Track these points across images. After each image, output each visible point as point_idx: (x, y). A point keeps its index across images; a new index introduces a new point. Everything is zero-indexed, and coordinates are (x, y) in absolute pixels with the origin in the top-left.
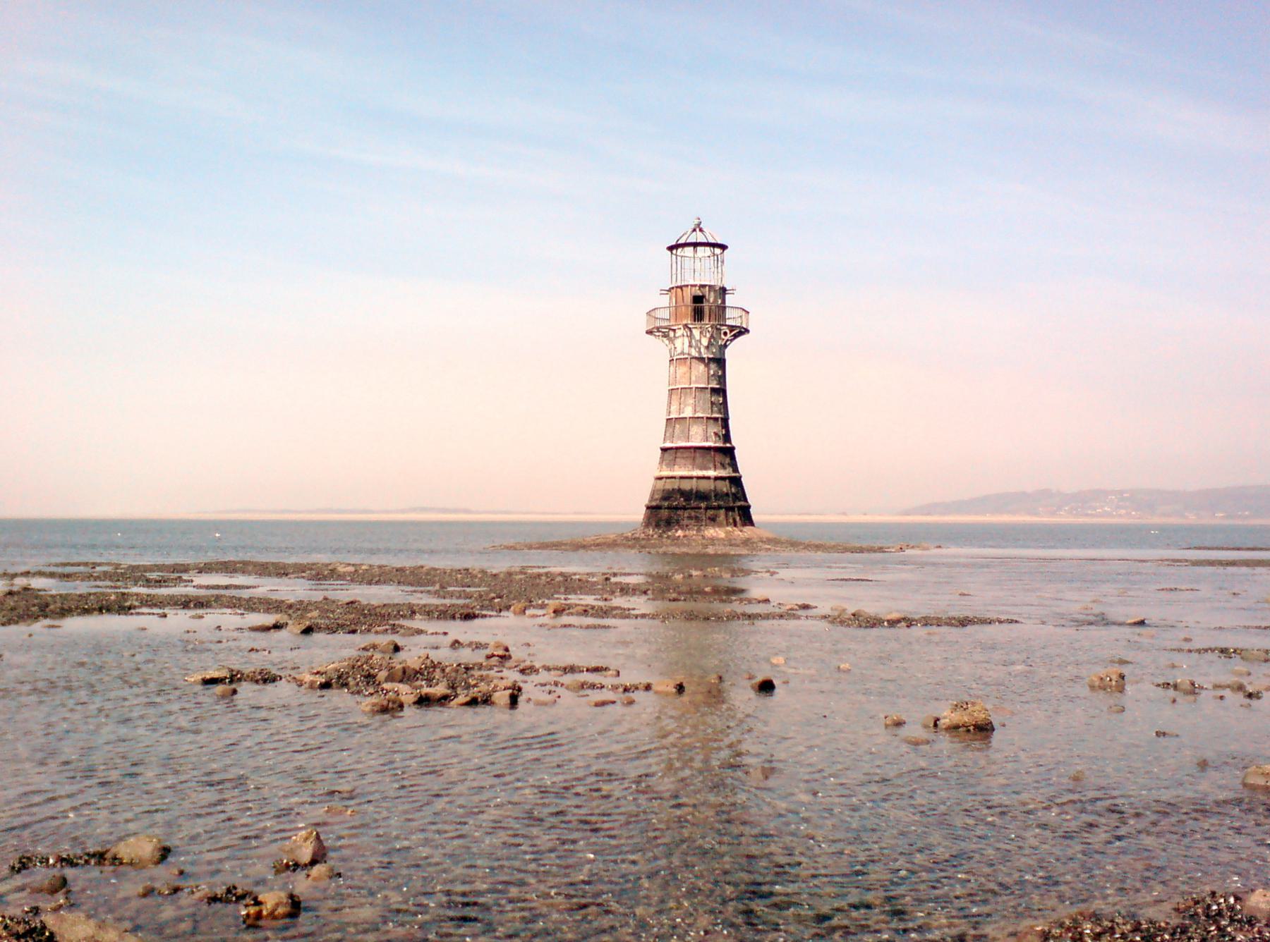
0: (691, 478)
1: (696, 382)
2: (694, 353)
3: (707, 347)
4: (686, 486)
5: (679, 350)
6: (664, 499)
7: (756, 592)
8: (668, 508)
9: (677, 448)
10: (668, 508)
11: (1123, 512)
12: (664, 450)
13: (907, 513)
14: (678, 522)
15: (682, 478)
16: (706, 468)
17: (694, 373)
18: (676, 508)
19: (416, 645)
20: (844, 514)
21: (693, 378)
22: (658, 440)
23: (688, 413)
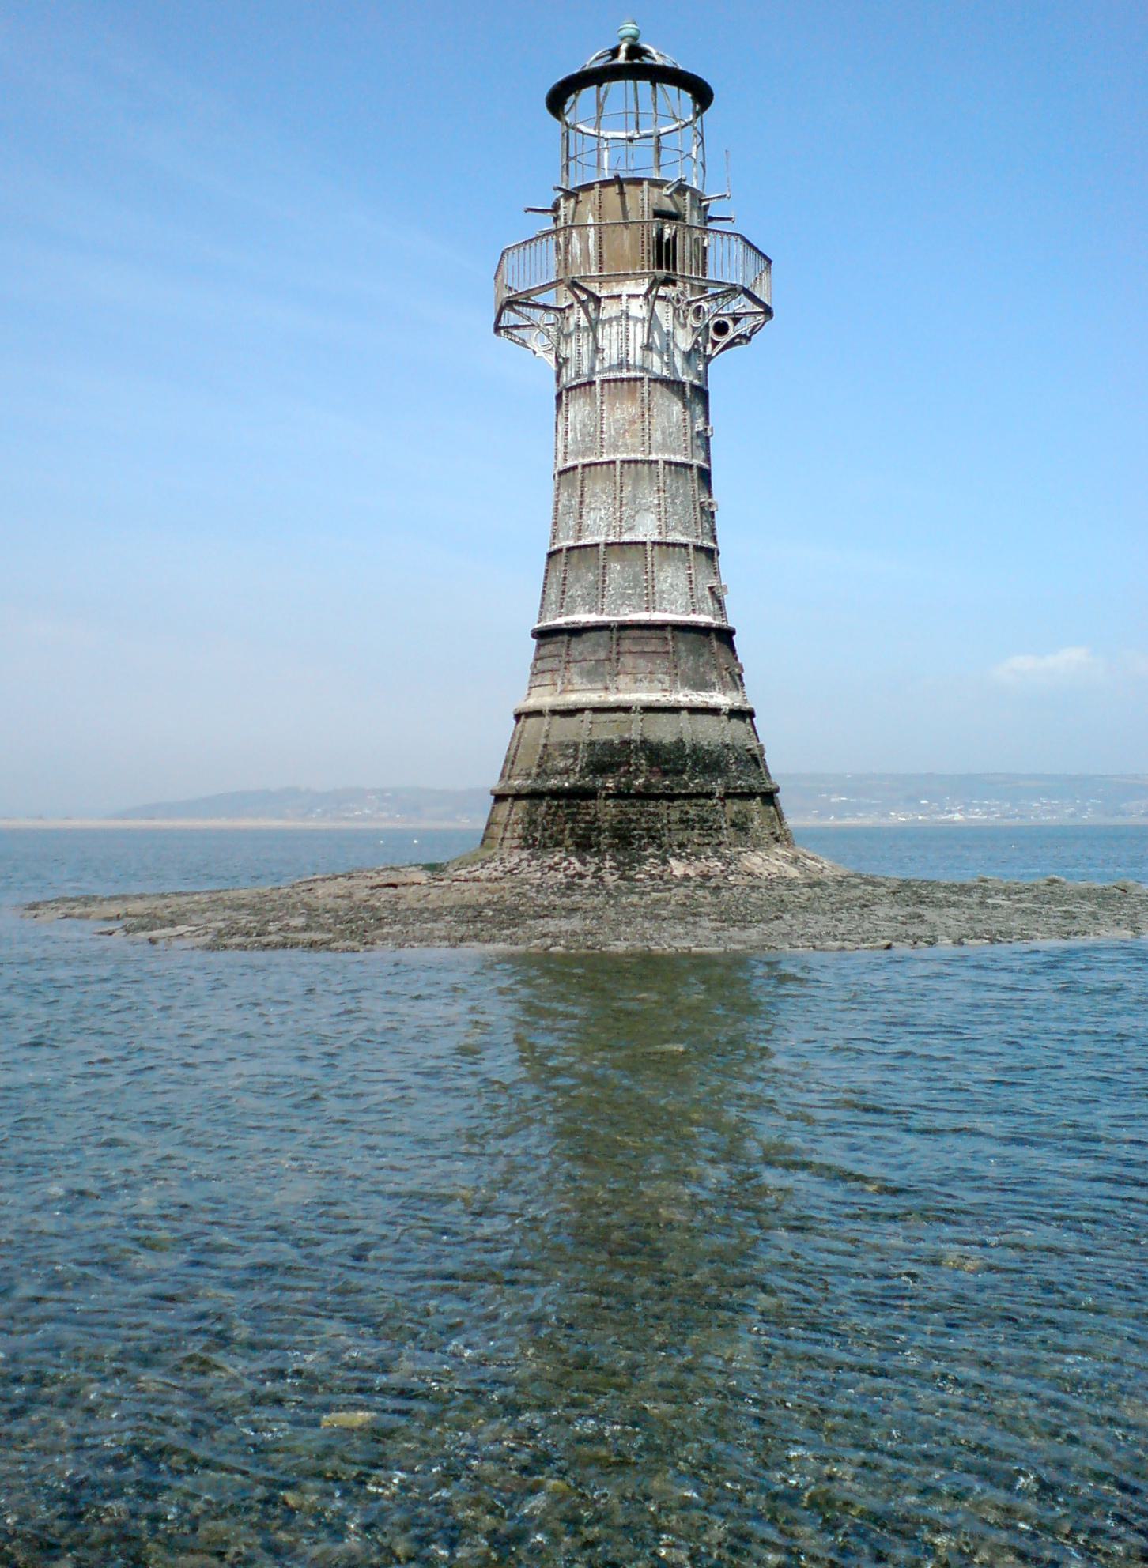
0: (675, 710)
1: (664, 447)
2: (657, 366)
3: (687, 356)
4: (663, 731)
5: (612, 355)
6: (600, 768)
7: (511, 1009)
8: (619, 795)
9: (624, 627)
10: (619, 795)
11: (385, 814)
12: (543, 635)
13: (124, 816)
14: (654, 837)
15: (648, 709)
16: (702, 685)
17: (658, 420)
18: (645, 795)
19: (164, 1281)
20: (40, 818)
21: (657, 436)
22: (520, 603)
23: (646, 530)
